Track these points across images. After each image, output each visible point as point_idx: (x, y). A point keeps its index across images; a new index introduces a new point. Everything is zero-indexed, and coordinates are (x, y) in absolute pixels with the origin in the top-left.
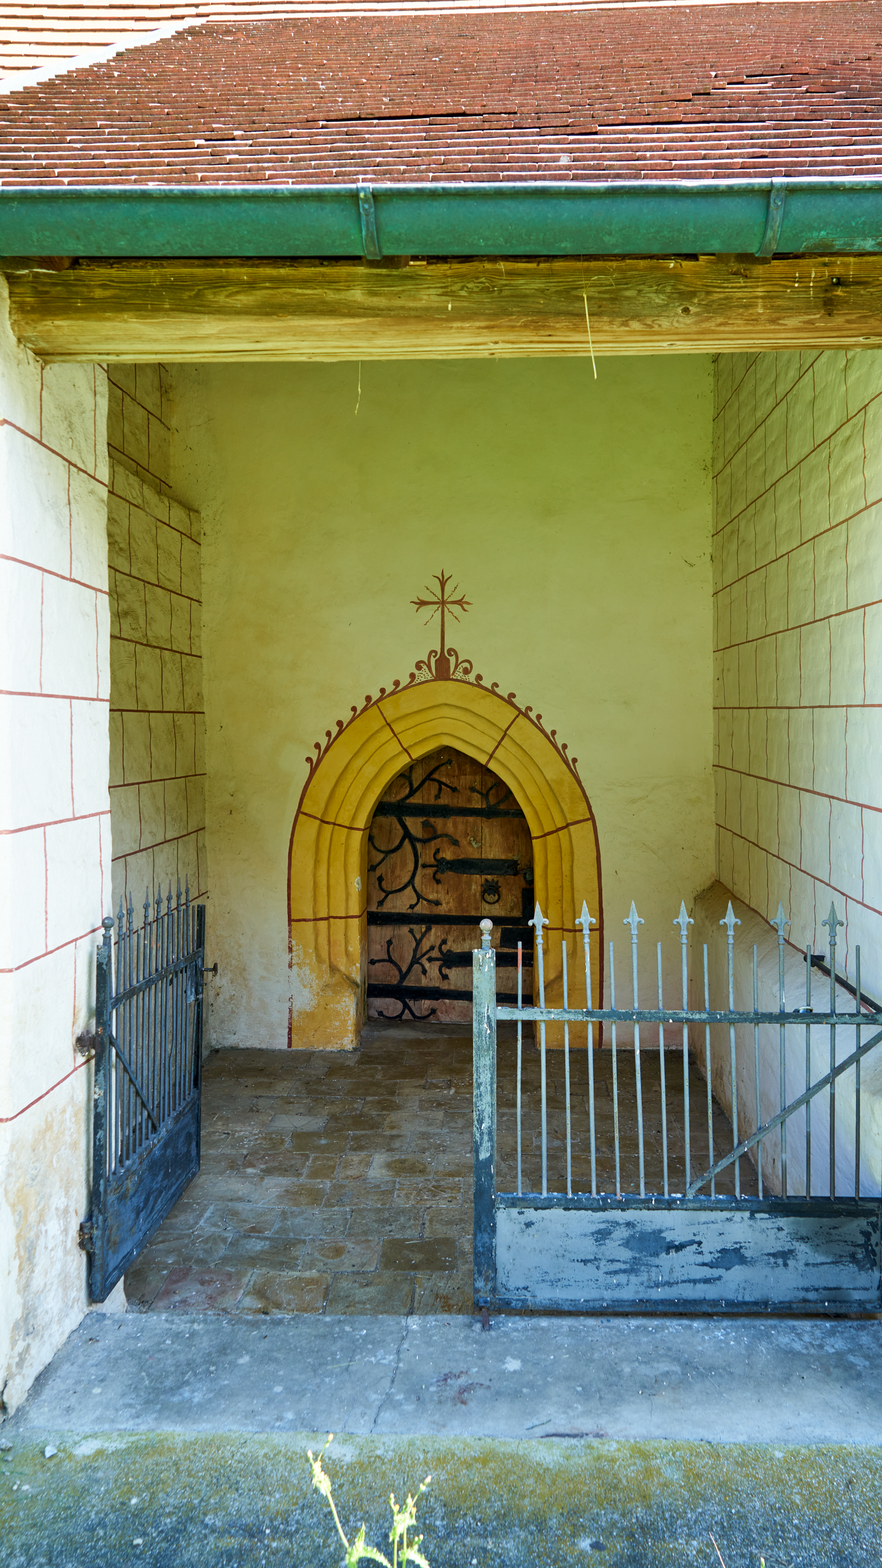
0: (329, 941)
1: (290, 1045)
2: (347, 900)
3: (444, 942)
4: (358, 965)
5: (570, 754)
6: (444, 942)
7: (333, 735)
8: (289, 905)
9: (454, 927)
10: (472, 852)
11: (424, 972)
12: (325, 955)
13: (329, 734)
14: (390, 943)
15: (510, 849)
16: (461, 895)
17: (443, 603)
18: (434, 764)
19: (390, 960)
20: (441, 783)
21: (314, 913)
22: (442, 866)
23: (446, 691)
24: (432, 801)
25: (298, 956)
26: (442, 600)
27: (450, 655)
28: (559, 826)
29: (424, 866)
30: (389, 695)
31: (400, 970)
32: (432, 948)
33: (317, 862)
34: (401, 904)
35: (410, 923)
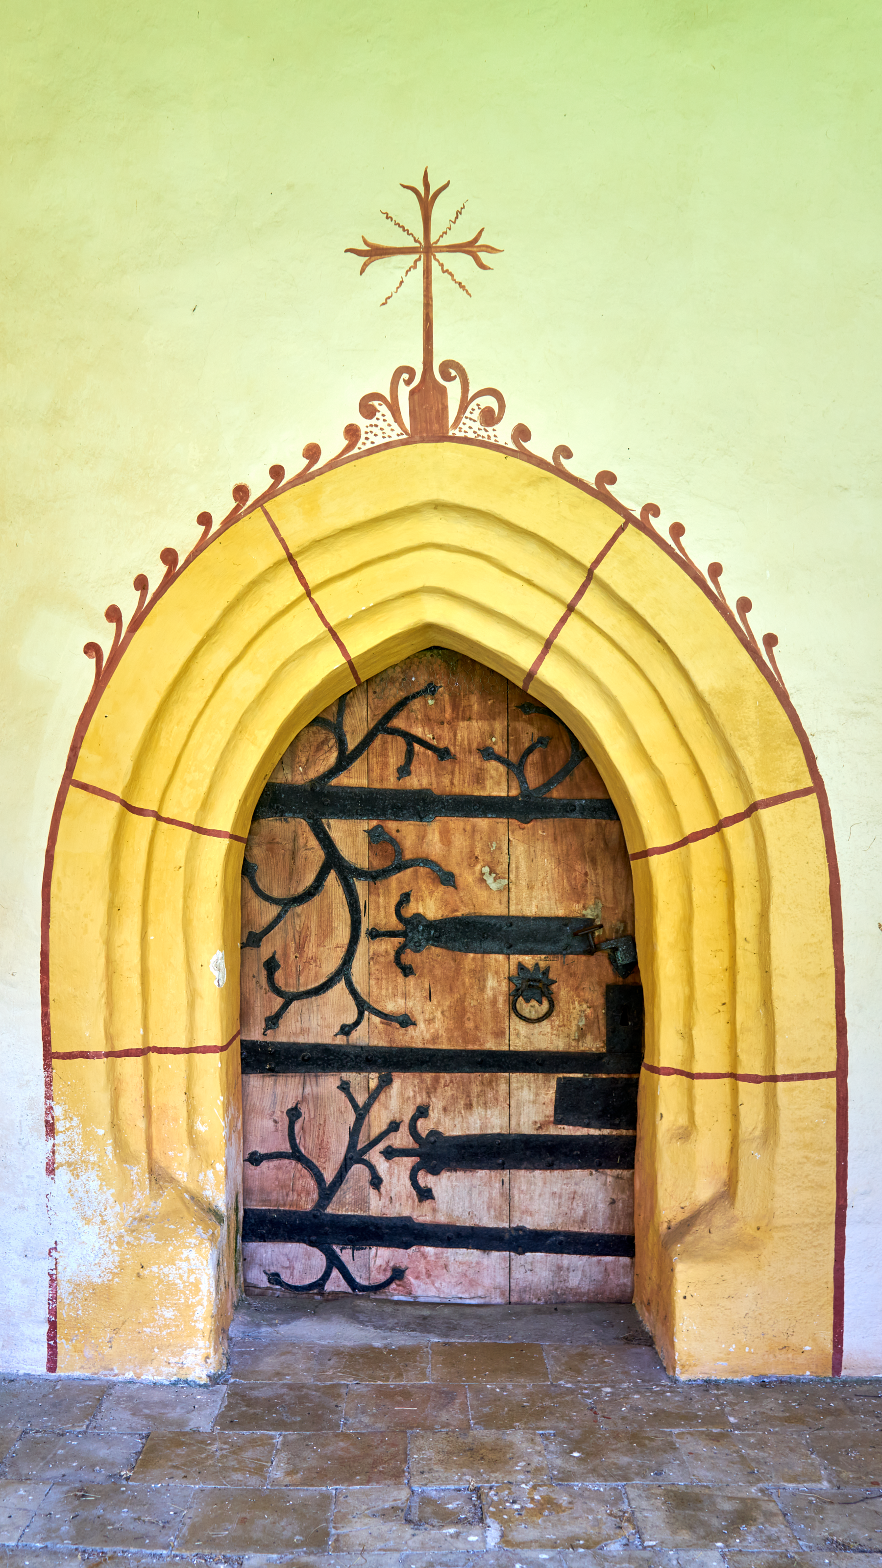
0: (148, 1107)
1: (52, 1366)
2: (191, 1005)
3: (422, 1112)
4: (220, 1167)
5: (758, 624)
6: (422, 1112)
7: (153, 586)
8: (45, 1015)
9: (446, 1077)
10: (485, 900)
11: (376, 1182)
12: (136, 1142)
13: (141, 583)
14: (294, 1114)
15: (577, 893)
16: (462, 1000)
17: (428, 250)
18: (394, 694)
19: (296, 1155)
20: (411, 739)
21: (109, 1037)
22: (415, 933)
23: (437, 469)
24: (391, 782)
25: (70, 1144)
26: (426, 241)
27: (448, 378)
28: (726, 812)
29: (375, 934)
30: (293, 483)
31: (318, 1177)
32: (394, 1126)
33: (114, 909)
34: (319, 1022)
35: (342, 1068)
